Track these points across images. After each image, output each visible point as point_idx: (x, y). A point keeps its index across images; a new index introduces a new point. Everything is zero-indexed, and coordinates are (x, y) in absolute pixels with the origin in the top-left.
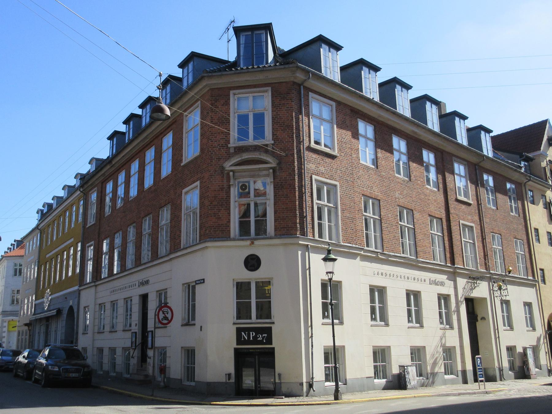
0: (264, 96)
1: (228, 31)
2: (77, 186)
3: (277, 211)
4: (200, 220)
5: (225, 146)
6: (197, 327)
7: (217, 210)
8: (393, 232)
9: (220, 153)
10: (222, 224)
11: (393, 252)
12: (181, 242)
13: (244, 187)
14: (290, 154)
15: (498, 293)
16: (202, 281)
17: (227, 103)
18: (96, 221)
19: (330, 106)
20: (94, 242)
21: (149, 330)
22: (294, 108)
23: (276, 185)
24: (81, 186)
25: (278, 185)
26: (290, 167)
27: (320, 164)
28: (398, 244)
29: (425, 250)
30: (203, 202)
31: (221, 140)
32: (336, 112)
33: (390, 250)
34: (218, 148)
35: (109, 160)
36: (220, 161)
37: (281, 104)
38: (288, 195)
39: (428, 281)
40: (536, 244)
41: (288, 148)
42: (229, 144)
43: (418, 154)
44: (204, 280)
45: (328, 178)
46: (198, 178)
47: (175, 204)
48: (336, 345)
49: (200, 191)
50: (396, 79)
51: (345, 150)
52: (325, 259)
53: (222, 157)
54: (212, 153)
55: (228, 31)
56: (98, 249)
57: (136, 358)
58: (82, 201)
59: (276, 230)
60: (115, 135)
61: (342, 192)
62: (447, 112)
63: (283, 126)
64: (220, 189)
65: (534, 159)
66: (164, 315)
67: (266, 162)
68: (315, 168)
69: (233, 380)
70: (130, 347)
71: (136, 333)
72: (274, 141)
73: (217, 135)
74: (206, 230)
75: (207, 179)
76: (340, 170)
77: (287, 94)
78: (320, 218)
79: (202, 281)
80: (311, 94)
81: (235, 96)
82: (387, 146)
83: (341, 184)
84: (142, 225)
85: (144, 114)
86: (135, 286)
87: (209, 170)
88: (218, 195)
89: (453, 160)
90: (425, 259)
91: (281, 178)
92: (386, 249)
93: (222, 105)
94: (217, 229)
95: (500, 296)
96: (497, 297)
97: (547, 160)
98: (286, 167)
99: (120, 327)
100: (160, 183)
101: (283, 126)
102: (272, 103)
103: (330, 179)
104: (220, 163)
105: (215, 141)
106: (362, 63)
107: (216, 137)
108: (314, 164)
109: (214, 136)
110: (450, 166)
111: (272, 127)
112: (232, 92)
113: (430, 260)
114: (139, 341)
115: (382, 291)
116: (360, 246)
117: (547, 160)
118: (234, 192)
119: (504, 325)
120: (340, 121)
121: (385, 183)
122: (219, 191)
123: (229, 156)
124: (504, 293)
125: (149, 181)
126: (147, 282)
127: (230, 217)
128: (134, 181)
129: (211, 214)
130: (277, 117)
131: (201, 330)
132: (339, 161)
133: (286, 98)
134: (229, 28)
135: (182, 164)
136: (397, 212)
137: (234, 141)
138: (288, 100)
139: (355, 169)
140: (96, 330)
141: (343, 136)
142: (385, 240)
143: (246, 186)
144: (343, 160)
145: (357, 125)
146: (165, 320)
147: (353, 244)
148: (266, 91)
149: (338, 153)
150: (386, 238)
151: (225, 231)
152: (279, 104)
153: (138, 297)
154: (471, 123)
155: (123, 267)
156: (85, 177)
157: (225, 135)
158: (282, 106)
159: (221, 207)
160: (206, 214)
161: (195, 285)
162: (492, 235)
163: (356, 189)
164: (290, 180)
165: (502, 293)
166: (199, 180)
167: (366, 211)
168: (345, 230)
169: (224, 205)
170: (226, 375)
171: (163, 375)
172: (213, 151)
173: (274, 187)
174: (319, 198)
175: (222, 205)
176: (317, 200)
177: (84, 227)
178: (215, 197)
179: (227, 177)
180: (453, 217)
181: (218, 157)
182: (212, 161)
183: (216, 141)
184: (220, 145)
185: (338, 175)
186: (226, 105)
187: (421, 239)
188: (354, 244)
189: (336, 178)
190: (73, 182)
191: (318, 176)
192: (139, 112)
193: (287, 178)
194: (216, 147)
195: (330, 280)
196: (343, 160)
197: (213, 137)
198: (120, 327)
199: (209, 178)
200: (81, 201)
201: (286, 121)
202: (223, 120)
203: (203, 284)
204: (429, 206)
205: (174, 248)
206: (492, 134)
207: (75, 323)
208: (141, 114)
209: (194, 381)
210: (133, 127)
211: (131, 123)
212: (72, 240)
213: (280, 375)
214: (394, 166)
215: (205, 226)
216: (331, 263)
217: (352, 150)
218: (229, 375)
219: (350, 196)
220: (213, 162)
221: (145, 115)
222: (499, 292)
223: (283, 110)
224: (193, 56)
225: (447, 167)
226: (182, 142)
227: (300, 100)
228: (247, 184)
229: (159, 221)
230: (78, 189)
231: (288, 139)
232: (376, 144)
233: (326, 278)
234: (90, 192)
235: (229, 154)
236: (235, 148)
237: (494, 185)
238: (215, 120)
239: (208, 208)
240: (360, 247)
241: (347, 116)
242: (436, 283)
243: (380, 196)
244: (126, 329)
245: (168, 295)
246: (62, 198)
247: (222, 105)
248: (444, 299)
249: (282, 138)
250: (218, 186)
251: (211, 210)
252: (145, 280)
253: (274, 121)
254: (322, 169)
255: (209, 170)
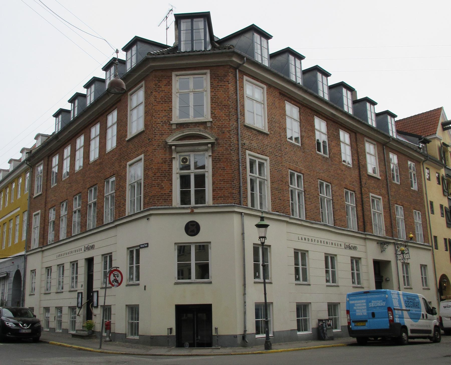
0: (203, 77)
1: (166, 19)
2: (22, 160)
3: (215, 182)
4: (144, 190)
5: (167, 123)
6: (142, 287)
7: (160, 180)
8: (314, 202)
9: (163, 129)
10: (165, 194)
11: (314, 220)
12: (125, 210)
13: (185, 160)
14: (227, 131)
15: (401, 257)
16: (146, 245)
17: (169, 84)
18: (42, 191)
19: (262, 89)
20: (41, 211)
21: (94, 290)
22: (231, 89)
23: (214, 159)
24: (28, 160)
25: (216, 159)
26: (227, 143)
27: (253, 140)
28: (319, 213)
29: (341, 219)
30: (147, 173)
31: (164, 117)
32: (267, 94)
33: (311, 218)
34: (161, 125)
35: (55, 137)
36: (163, 136)
37: (218, 86)
38: (224, 168)
39: (343, 246)
40: (431, 215)
41: (225, 125)
42: (172, 120)
43: (336, 134)
44: (148, 244)
45: (259, 154)
46: (142, 152)
47: (120, 175)
48: (267, 301)
49: (144, 164)
50: (317, 67)
51: (274, 128)
52: (258, 226)
53: (164, 132)
54: (156, 129)
55: (166, 19)
56: (45, 217)
57: (82, 316)
58: (29, 173)
59: (214, 199)
60: (60, 113)
61: (272, 166)
62: (358, 99)
63: (220, 106)
64: (163, 162)
65: (431, 142)
66: (114, 278)
67: (205, 138)
68: (249, 144)
69: (174, 333)
70: (76, 306)
71: (82, 293)
72: (213, 118)
73: (161, 113)
74: (150, 199)
75: (151, 152)
76: (270, 146)
77: (224, 76)
78: (252, 189)
79: (146, 245)
80: (245, 78)
81: (177, 77)
82: (310, 127)
83: (271, 159)
84: (88, 195)
85: (89, 94)
86: (81, 250)
87: (153, 144)
88: (161, 167)
89: (365, 140)
90: (341, 227)
91: (218, 153)
92: (308, 218)
93: (165, 85)
94: (160, 198)
95: (402, 260)
96: (400, 260)
97: (441, 142)
98: (223, 142)
99: (67, 288)
100: (105, 156)
101: (220, 106)
102: (211, 85)
103: (261, 154)
104: (163, 138)
105: (159, 118)
106: (288, 51)
107: (159, 114)
108: (248, 141)
109: (157, 114)
110: (362, 146)
111: (211, 106)
112: (174, 74)
113: (345, 228)
114: (85, 300)
115: (304, 253)
116: (287, 214)
117: (441, 142)
118: (176, 165)
119: (256, 277)
120: (270, 103)
121: (308, 159)
122: (162, 163)
123: (171, 132)
124: (406, 256)
125: (94, 155)
126: (93, 247)
127: (172, 188)
128: (80, 155)
129: (155, 184)
130: (215, 97)
131: (145, 289)
132: (269, 138)
133: (223, 80)
134: (167, 16)
135: (127, 139)
136: (318, 185)
137: (176, 118)
138: (225, 82)
139: (283, 146)
140: (43, 291)
141: (273, 116)
142: (307, 209)
143: (186, 159)
144: (272, 137)
145: (285, 107)
146: (115, 282)
147: (280, 212)
148: (205, 74)
149: (268, 131)
150: (308, 207)
151: (168, 199)
152: (217, 86)
153: (84, 260)
154: (379, 109)
155: (69, 234)
156: (31, 151)
157: (168, 112)
158: (219, 87)
159: (164, 178)
160: (150, 185)
161: (139, 249)
162: (396, 206)
163: (283, 164)
164: (227, 154)
165: (405, 257)
166: (143, 153)
167: (291, 184)
168: (274, 200)
169: (167, 176)
170: (168, 329)
171: (108, 331)
172: (156, 127)
173: (213, 161)
174: (251, 171)
175: (164, 176)
176: (250, 173)
177: (30, 197)
178: (158, 169)
179: (169, 151)
180: (365, 190)
181: (161, 132)
182: (156, 136)
183: (159, 118)
184: (163, 121)
185: (268, 151)
186: (168, 85)
187: (338, 209)
188: (282, 213)
189: (266, 154)
190: (18, 156)
191: (252, 151)
192: (84, 91)
193: (224, 152)
194: (159, 123)
195: (263, 243)
196: (272, 137)
197: (156, 115)
198: (67, 288)
199: (153, 152)
200: (27, 173)
201: (223, 101)
202: (166, 99)
203: (146, 248)
204: (345, 180)
205: (119, 215)
206: (396, 119)
207: (22, 285)
208: (86, 93)
209: (138, 335)
210: (78, 106)
211: (76, 102)
212: (19, 209)
213: (216, 329)
214: (316, 144)
215: (149, 195)
216: (263, 229)
217: (281, 129)
218: (171, 329)
219: (278, 170)
220: (157, 137)
221: (90, 94)
222: (402, 255)
223: (220, 91)
224: (137, 41)
225: (360, 146)
226: (127, 118)
227: (236, 82)
228: (188, 157)
229: (104, 191)
230: (24, 161)
231: (225, 117)
232: (300, 124)
233: (259, 242)
234: (37, 165)
235: (172, 130)
236: (177, 124)
237: (398, 163)
238: (158, 98)
239: (152, 179)
240: (286, 215)
241: (276, 98)
242: (349, 247)
243: (304, 171)
244: (59, 291)
245: (113, 258)
246: (8, 171)
247: (165, 85)
248: (355, 261)
249: (219, 116)
250: (162, 159)
251: (155, 180)
252: (91, 245)
253: (212, 101)
254: (254, 144)
255: (153, 144)
